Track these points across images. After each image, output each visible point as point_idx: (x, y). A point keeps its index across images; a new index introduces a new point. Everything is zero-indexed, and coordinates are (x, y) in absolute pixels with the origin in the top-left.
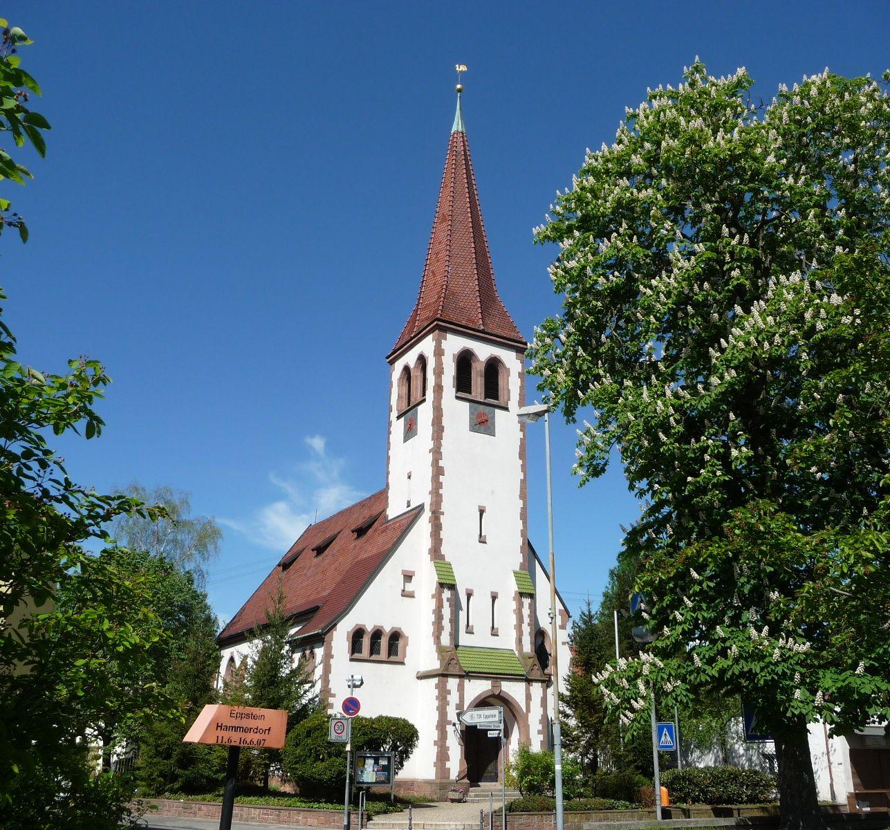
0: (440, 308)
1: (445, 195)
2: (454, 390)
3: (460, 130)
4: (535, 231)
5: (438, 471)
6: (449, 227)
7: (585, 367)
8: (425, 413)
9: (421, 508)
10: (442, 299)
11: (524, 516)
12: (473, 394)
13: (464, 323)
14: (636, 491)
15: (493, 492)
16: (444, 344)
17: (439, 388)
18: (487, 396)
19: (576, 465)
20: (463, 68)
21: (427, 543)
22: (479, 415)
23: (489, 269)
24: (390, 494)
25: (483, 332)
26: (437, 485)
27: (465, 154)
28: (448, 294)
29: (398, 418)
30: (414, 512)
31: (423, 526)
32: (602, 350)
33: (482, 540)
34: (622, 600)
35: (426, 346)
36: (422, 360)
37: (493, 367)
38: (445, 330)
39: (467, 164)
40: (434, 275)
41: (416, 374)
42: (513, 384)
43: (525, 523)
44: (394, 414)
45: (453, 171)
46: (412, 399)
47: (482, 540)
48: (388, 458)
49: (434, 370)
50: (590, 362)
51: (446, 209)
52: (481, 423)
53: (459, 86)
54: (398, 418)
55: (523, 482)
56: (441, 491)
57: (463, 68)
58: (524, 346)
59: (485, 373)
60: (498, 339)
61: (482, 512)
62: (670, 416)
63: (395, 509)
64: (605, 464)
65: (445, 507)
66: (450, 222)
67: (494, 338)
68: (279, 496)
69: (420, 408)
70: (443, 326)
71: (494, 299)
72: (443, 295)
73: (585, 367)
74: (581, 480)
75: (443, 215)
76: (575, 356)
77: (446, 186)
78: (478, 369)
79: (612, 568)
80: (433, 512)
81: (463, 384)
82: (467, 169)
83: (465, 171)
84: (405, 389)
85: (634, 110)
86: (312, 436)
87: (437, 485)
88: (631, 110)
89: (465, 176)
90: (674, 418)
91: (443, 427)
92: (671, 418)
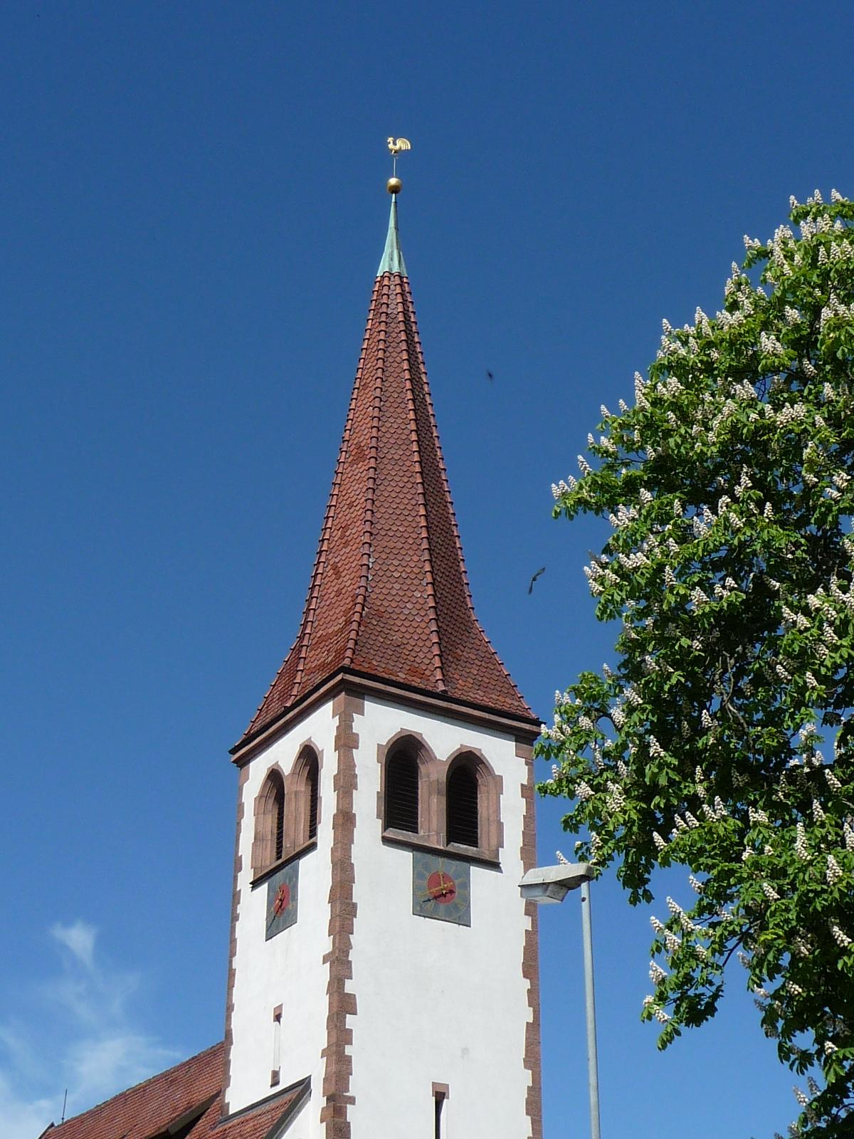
0: (351, 644)
1: (364, 405)
2: (380, 823)
3: (396, 269)
4: (556, 490)
5: (342, 1005)
7: (663, 781)
9: (302, 1088)
10: (355, 626)
12: (421, 832)
13: (401, 677)
15: (465, 1051)
16: (359, 724)
17: (345, 820)
18: (451, 838)
20: (403, 144)
22: (435, 880)
23: (456, 561)
25: (443, 696)
26: (339, 1037)
27: (407, 321)
29: (255, 884)
30: (287, 1097)
36: (309, 757)
38: (360, 693)
40: (338, 574)
41: (296, 789)
44: (246, 876)
45: (381, 354)
46: (286, 843)
48: (231, 974)
51: (364, 435)
52: (439, 897)
53: (393, 181)
54: (255, 884)
55: (533, 1028)
56: (348, 1050)
57: (403, 144)
58: (534, 728)
61: (440, 1097)
64: (715, 996)
65: (356, 1086)
69: (305, 863)
72: (356, 617)
73: (663, 781)
75: (359, 447)
78: (434, 777)
80: (331, 1098)
82: (411, 351)
84: (270, 822)
85: (764, 243)
86: (68, 923)
87: (339, 1037)
89: (406, 366)
91: (355, 905)
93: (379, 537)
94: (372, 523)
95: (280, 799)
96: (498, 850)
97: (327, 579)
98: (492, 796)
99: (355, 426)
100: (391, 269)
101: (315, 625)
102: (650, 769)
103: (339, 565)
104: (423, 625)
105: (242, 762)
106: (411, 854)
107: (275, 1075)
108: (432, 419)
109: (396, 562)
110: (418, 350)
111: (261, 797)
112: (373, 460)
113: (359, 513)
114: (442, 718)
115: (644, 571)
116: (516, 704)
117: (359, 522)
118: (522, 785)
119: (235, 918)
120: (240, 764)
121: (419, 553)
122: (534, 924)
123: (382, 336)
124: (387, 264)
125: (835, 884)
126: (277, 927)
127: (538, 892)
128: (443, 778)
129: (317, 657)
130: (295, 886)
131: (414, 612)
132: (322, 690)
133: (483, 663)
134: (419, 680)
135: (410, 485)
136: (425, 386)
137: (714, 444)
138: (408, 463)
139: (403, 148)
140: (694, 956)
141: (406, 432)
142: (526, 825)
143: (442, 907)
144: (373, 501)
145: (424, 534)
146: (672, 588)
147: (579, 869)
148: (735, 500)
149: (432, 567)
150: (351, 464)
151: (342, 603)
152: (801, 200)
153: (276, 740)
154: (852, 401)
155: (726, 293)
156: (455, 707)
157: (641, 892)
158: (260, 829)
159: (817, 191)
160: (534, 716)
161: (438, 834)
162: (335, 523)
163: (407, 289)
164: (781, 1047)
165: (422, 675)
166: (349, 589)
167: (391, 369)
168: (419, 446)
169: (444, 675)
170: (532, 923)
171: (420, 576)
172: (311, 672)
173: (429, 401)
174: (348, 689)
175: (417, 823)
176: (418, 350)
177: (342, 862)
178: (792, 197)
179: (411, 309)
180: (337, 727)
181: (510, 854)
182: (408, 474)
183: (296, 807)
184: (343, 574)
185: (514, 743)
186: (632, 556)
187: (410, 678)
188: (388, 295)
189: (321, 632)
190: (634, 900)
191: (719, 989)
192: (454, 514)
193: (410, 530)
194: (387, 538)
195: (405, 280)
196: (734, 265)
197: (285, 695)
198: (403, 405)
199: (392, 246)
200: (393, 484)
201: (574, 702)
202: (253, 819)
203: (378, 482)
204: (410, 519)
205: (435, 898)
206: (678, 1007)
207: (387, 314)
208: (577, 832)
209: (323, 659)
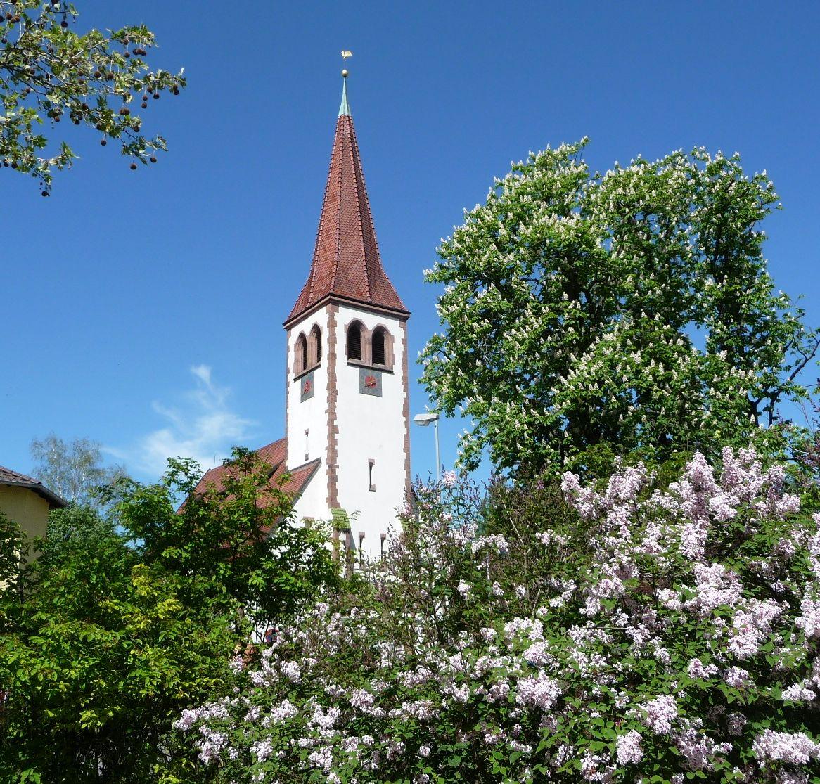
0: (333, 283)
1: (335, 176)
2: (346, 357)
3: (346, 114)
4: (425, 272)
5: (333, 430)
6: (339, 207)
7: (463, 385)
8: (320, 378)
9: (318, 461)
10: (334, 275)
13: (353, 296)
16: (337, 316)
17: (332, 356)
18: (374, 362)
19: (457, 461)
20: (347, 54)
21: (325, 493)
22: (368, 379)
23: (374, 244)
24: (289, 447)
25: (370, 304)
26: (332, 443)
27: (352, 138)
28: (340, 271)
29: (296, 380)
30: (312, 465)
31: (321, 478)
32: (476, 371)
33: (372, 489)
35: (321, 317)
36: (317, 330)
37: (380, 334)
38: (337, 303)
41: (311, 342)
42: (396, 350)
44: (291, 376)
46: (308, 364)
47: (372, 489)
48: (287, 415)
49: (328, 339)
51: (335, 189)
53: (345, 72)
54: (296, 380)
55: (407, 436)
56: (336, 448)
57: (347, 54)
58: (407, 315)
60: (383, 310)
61: (371, 465)
63: (294, 461)
66: (339, 202)
67: (378, 309)
68: (160, 424)
69: (316, 372)
70: (335, 300)
72: (334, 271)
77: (335, 167)
81: (353, 351)
82: (354, 151)
83: (351, 153)
84: (301, 354)
86: (198, 365)
87: (332, 443)
89: (352, 158)
90: (528, 434)
91: (337, 391)
92: (525, 434)
107: (307, 456)
119: (287, 393)
122: (407, 395)
128: (370, 337)
129: (318, 287)
130: (312, 382)
140: (472, 449)
147: (434, 416)
150: (330, 202)
152: (516, 163)
156: (375, 308)
165: (361, 295)
181: (398, 368)
183: (312, 349)
190: (448, 416)
197: (305, 302)
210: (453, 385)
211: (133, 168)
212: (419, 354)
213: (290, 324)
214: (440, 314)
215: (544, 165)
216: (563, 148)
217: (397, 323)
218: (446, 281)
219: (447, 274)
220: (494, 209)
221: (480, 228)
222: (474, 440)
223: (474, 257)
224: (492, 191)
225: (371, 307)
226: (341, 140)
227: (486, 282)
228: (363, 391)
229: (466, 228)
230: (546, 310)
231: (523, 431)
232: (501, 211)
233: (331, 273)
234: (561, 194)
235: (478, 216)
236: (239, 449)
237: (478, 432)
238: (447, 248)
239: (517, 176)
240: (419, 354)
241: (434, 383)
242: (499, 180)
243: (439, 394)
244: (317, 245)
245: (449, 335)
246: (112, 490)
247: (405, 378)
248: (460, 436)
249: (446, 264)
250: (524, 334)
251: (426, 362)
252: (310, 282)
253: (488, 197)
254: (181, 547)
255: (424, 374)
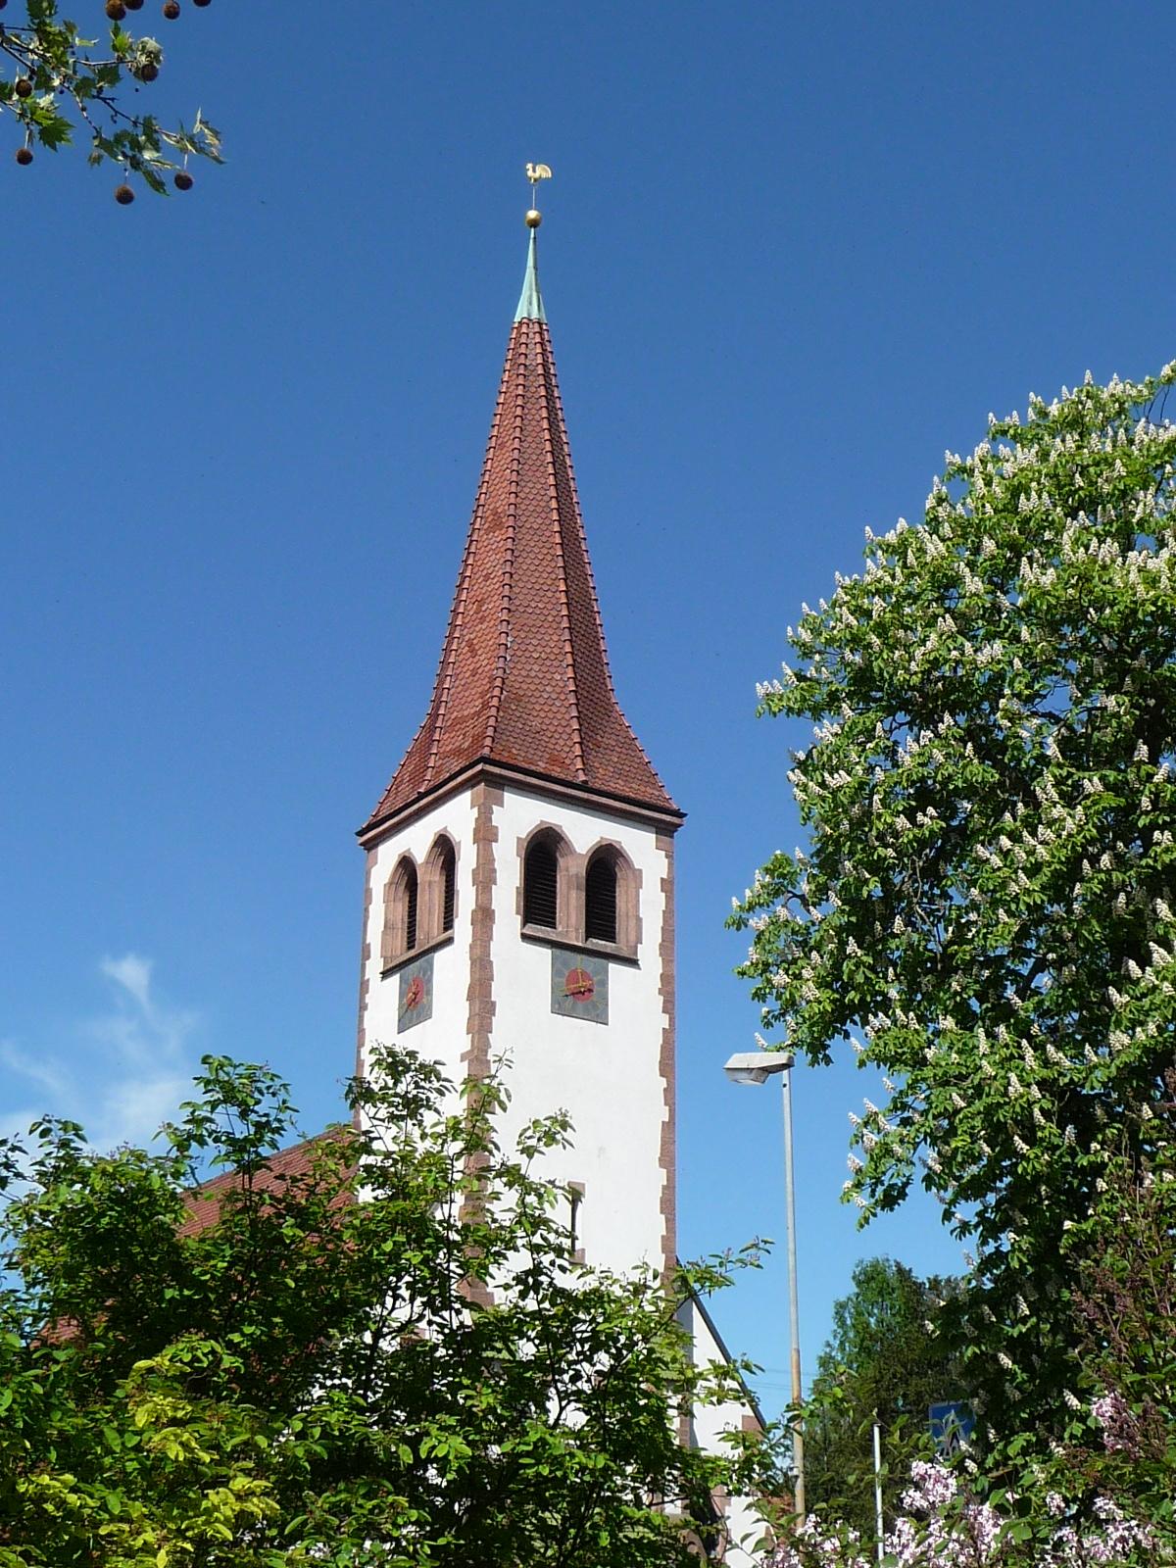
0: (490, 731)
1: (501, 465)
2: (519, 919)
3: (535, 315)
4: (760, 690)
7: (860, 979)
8: (450, 970)
10: (493, 711)
11: (668, 1205)
12: (560, 928)
13: (541, 767)
14: (955, 1223)
16: (498, 816)
17: (484, 916)
18: (589, 934)
19: (848, 1184)
20: (542, 172)
22: (573, 977)
23: (597, 639)
25: (583, 787)
27: (546, 375)
28: (508, 701)
29: (386, 974)
34: (883, 1394)
35: (457, 816)
36: (445, 849)
37: (605, 865)
38: (499, 783)
39: (550, 397)
40: (473, 652)
41: (430, 880)
43: (670, 1222)
44: (375, 966)
45: (519, 411)
46: (419, 935)
50: (872, 968)
51: (502, 501)
52: (577, 993)
53: (532, 214)
54: (386, 974)
55: (669, 1127)
57: (542, 172)
59: (587, 885)
62: (1035, 1102)
64: (906, 1184)
67: (604, 800)
69: (439, 957)
71: (608, 709)
73: (860, 979)
74: (860, 1215)
76: (840, 956)
77: (502, 445)
78: (573, 871)
79: (843, 1299)
81: (538, 904)
82: (551, 409)
84: (401, 909)
85: (964, 459)
86: (118, 955)
88: (957, 459)
89: (545, 424)
90: (1042, 1110)
91: (493, 1004)
92: (1037, 1112)
93: (517, 614)
94: (510, 599)
95: (412, 887)
96: (636, 947)
97: (462, 657)
98: (632, 890)
99: (491, 489)
100: (529, 315)
101: (449, 705)
102: (847, 966)
103: (475, 642)
104: (563, 710)
105: (371, 845)
106: (550, 951)
108: (572, 483)
109: (535, 642)
110: (558, 406)
111: (391, 883)
112: (511, 529)
113: (496, 586)
114: (582, 809)
115: (847, 790)
116: (657, 793)
117: (496, 597)
118: (662, 879)
119: (363, 1007)
120: (368, 846)
121: (559, 632)
123: (520, 390)
124: (525, 309)
125: (1016, 1099)
126: (410, 1021)
127: (744, 1075)
129: (448, 741)
130: (430, 980)
131: (554, 696)
132: (460, 779)
133: (624, 750)
134: (559, 770)
135: (549, 558)
136: (565, 446)
137: (916, 673)
138: (548, 534)
139: (544, 176)
141: (546, 498)
142: (665, 920)
143: (580, 1005)
144: (511, 575)
145: (565, 612)
146: (879, 816)
147: (781, 1058)
148: (937, 735)
149: (573, 647)
151: (478, 684)
153: (408, 825)
154: (1170, 1227)
155: (928, 507)
156: (595, 798)
157: (821, 1056)
158: (390, 917)
159: (1015, 413)
160: (675, 807)
161: (577, 930)
162: (470, 595)
163: (546, 337)
164: (946, 1211)
166: (486, 669)
167: (530, 428)
168: (559, 514)
169: (584, 764)
170: (670, 1021)
171: (560, 658)
172: (446, 756)
173: (569, 464)
174: (490, 781)
175: (555, 918)
176: (558, 406)
177: (482, 960)
178: (991, 415)
179: (550, 360)
180: (477, 819)
181: (649, 952)
182: (548, 545)
184: (479, 653)
185: (654, 836)
186: (836, 776)
187: (551, 768)
188: (527, 345)
189: (455, 714)
190: (814, 1062)
191: (909, 1178)
192: (594, 588)
193: (549, 606)
194: (526, 615)
195: (544, 327)
196: (936, 478)
198: (542, 469)
199: (531, 289)
200: (532, 556)
201: (764, 878)
202: (383, 906)
203: (516, 553)
204: (550, 594)
205: (573, 994)
206: (873, 1191)
207: (525, 365)
208: (764, 1001)
209: (458, 744)
210: (831, 979)
211: (125, 198)
212: (735, 902)
213: (374, 834)
214: (802, 796)
215: (1075, 423)
216: (1116, 387)
217: (649, 838)
218: (817, 712)
219: (821, 695)
220: (946, 530)
221: (913, 574)
222: (892, 1127)
223: (892, 648)
224: (938, 487)
225: (585, 795)
226: (521, 380)
227: (925, 718)
228: (559, 1008)
229: (874, 570)
230: (1092, 784)
231: (1030, 1104)
232: (964, 536)
233: (486, 706)
234: (1124, 493)
235: (899, 550)
236: (391, 1053)
237: (905, 1107)
238: (816, 632)
239: (1004, 450)
240: (735, 902)
241: (780, 978)
242: (957, 459)
243: (791, 1005)
244: (450, 638)
245: (818, 853)
246: (15, 1156)
247: (666, 979)
248: (856, 1118)
249: (811, 672)
250: (1043, 845)
251: (759, 922)
252: (431, 728)
253: (930, 502)
254: (215, 1333)
255: (753, 954)
